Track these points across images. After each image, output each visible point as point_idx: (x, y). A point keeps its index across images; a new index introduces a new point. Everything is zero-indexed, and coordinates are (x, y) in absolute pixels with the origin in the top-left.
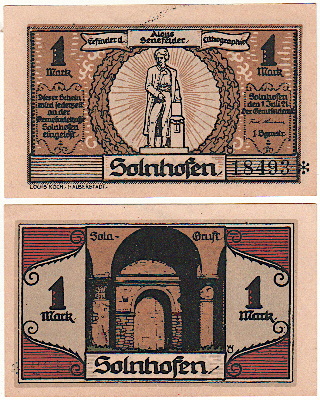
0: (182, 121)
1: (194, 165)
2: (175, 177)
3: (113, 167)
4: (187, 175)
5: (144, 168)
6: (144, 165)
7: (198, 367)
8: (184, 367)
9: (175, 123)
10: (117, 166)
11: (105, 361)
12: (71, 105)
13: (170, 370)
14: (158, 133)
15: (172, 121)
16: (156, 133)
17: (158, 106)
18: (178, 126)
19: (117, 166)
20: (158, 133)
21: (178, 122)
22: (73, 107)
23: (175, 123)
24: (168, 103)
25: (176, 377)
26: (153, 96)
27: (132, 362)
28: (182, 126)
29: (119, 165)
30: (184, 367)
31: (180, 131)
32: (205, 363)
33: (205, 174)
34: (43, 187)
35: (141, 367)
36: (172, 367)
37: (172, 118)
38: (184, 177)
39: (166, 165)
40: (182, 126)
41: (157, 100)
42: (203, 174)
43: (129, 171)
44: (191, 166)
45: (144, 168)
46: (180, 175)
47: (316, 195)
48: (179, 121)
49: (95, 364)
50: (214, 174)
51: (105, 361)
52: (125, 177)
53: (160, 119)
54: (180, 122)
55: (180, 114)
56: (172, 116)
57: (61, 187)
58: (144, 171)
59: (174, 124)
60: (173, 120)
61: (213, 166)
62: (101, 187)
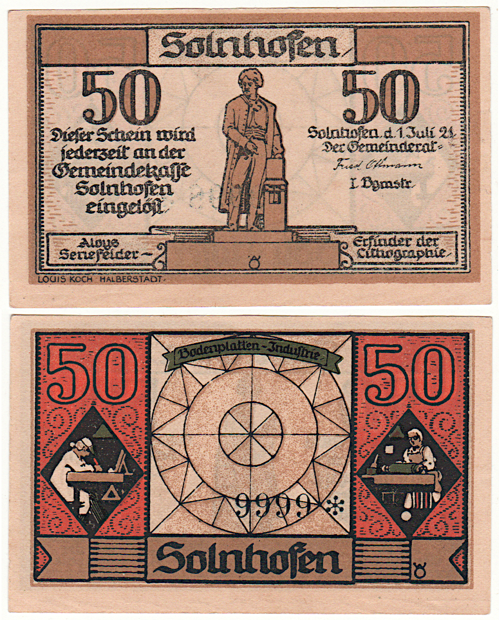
0: (283, 187)
1: (303, 553)
2: (271, 576)
3: (160, 556)
4: (291, 573)
5: (218, 558)
6: (218, 551)
7: (325, 47)
8: (307, 562)
9: (271, 189)
10: (168, 555)
11: (174, 550)
12: (99, 153)
13: (285, 568)
14: (244, 208)
15: (267, 187)
16: (240, 209)
17: (243, 163)
18: (276, 195)
19: (168, 555)
20: (244, 208)
21: (277, 189)
22: (103, 157)
23: (271, 189)
24: (260, 159)
25: (296, 579)
26: (236, 145)
27: (223, 552)
28: (283, 194)
29: (173, 554)
30: (307, 562)
31: (280, 203)
32: (338, 554)
33: (320, 54)
34: (60, 279)
35: (238, 562)
36: (290, 564)
37: (268, 182)
38: (286, 575)
39: (257, 553)
40: (283, 194)
41: (244, 152)
42: (317, 571)
43: (191, 564)
44: (299, 555)
45: (218, 558)
46: (279, 572)
47: (490, 303)
48: (279, 186)
49: (158, 557)
50: (335, 54)
51: (174, 550)
52: (183, 574)
53: (247, 184)
54: (280, 188)
55: (281, 176)
56: (267, 179)
57: (88, 279)
58: (217, 566)
59: (270, 192)
60: (267, 185)
61: (333, 41)
62: (154, 279)
